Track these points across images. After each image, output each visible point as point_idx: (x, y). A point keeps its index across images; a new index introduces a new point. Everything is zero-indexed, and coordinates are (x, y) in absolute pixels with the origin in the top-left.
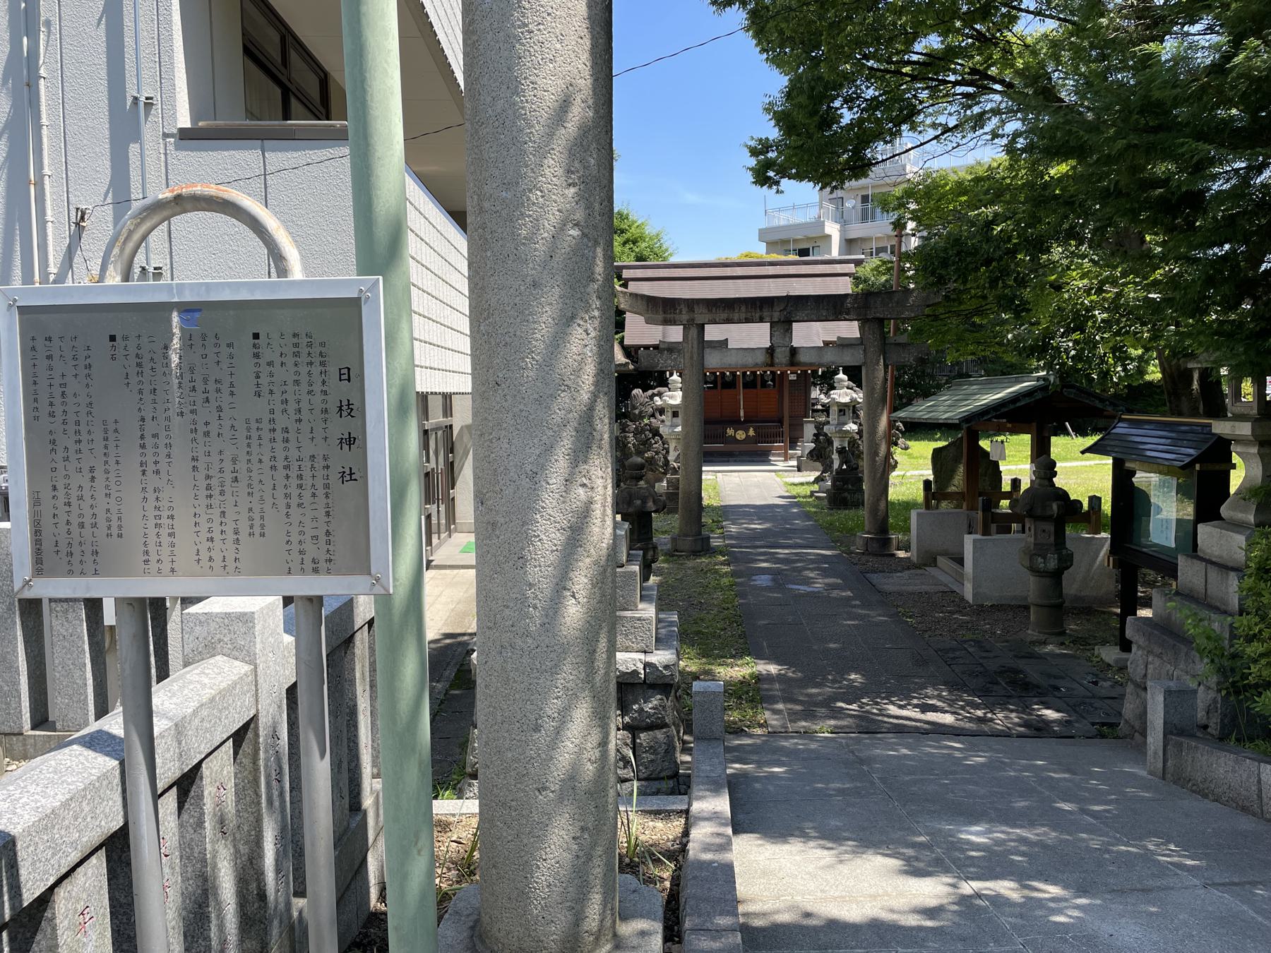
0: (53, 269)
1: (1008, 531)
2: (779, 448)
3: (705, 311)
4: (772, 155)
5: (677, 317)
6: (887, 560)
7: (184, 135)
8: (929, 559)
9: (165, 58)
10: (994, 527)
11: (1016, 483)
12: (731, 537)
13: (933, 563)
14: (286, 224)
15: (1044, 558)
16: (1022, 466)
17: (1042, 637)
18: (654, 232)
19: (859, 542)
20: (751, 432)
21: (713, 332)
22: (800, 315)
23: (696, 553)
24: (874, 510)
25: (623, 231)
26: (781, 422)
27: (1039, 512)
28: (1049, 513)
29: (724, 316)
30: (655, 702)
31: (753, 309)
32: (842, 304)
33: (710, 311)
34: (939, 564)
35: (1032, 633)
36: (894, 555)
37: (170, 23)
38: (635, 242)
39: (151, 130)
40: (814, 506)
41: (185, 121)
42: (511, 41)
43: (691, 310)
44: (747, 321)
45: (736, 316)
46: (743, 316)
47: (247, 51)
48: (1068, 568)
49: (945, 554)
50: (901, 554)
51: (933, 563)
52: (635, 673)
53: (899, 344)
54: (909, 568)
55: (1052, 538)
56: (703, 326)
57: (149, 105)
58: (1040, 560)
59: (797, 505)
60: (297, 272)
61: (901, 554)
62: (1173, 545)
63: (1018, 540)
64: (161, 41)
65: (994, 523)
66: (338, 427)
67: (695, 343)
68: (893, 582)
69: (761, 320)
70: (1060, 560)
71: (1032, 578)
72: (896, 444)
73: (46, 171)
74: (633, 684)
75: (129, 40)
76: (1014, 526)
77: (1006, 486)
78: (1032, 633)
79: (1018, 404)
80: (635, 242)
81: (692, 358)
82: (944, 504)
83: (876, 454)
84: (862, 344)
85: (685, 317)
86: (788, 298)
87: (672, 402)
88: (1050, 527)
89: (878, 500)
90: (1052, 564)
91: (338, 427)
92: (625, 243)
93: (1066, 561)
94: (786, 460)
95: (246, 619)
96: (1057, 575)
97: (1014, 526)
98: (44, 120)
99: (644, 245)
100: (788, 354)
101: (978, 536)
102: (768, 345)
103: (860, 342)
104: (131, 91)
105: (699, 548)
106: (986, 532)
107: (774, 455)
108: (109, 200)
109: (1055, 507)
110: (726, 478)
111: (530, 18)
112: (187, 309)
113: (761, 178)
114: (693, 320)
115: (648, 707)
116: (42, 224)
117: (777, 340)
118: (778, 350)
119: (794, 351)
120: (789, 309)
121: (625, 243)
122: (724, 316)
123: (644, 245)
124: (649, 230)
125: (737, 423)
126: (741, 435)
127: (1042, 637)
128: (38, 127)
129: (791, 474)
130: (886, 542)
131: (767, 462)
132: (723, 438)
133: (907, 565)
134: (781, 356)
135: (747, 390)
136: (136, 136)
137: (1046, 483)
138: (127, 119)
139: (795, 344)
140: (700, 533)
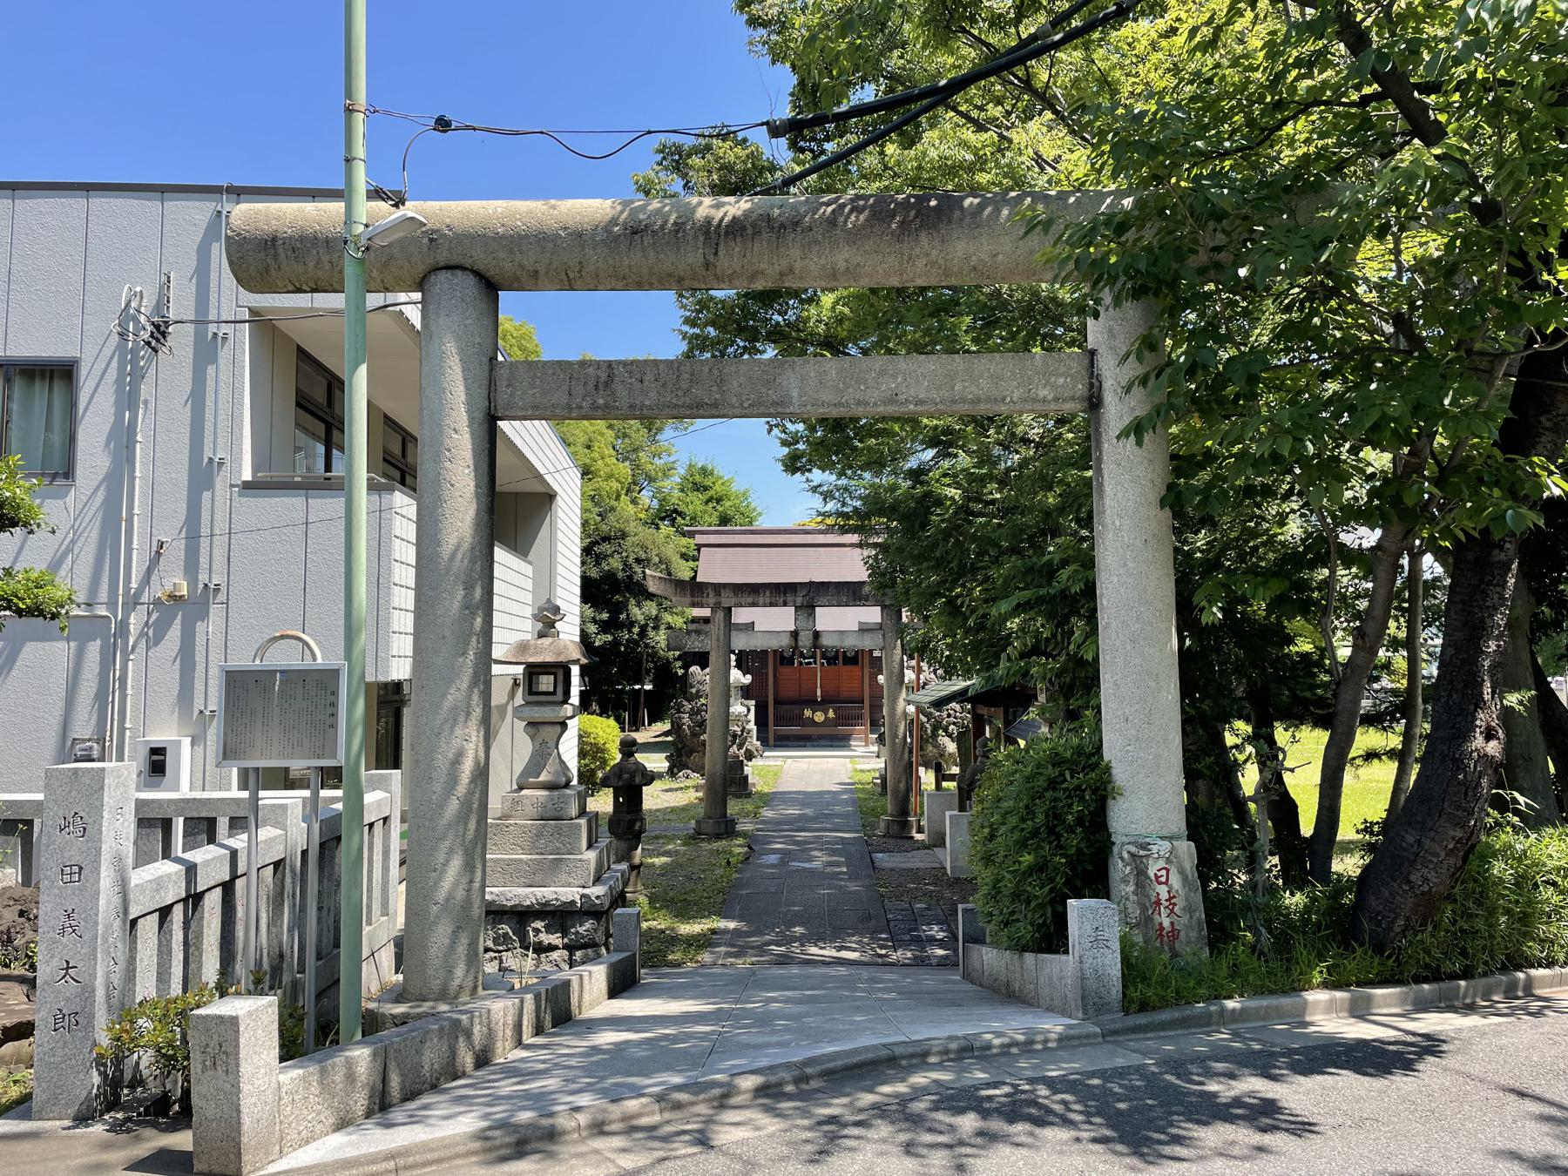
0: (134, 585)
2: (860, 732)
4: (801, 446)
7: (247, 486)
9: (236, 430)
12: (762, 822)
14: (318, 643)
18: (742, 489)
19: (882, 825)
20: (831, 714)
21: (741, 615)
22: (823, 600)
23: (718, 837)
25: (706, 489)
29: (750, 600)
30: (587, 925)
31: (778, 593)
33: (736, 595)
37: (242, 404)
38: (719, 500)
39: (221, 483)
41: (247, 475)
42: (437, 522)
43: (718, 594)
44: (772, 605)
45: (761, 600)
46: (768, 600)
47: (298, 404)
50: (919, 837)
52: (573, 902)
56: (729, 609)
57: (221, 464)
60: (319, 661)
61: (919, 837)
64: (235, 419)
66: (330, 710)
69: (785, 604)
73: (136, 511)
74: (572, 913)
75: (209, 416)
80: (719, 500)
85: (712, 600)
86: (811, 583)
91: (330, 710)
92: (707, 503)
95: (284, 807)
98: (138, 474)
99: (728, 504)
103: (880, 627)
104: (208, 453)
108: (183, 535)
111: (448, 512)
112: (282, 672)
115: (581, 930)
116: (129, 550)
119: (817, 635)
121: (707, 503)
122: (750, 600)
123: (728, 504)
124: (736, 487)
125: (812, 703)
126: (819, 717)
128: (132, 478)
130: (905, 825)
131: (847, 747)
133: (923, 846)
134: (805, 641)
136: (210, 486)
138: (202, 474)
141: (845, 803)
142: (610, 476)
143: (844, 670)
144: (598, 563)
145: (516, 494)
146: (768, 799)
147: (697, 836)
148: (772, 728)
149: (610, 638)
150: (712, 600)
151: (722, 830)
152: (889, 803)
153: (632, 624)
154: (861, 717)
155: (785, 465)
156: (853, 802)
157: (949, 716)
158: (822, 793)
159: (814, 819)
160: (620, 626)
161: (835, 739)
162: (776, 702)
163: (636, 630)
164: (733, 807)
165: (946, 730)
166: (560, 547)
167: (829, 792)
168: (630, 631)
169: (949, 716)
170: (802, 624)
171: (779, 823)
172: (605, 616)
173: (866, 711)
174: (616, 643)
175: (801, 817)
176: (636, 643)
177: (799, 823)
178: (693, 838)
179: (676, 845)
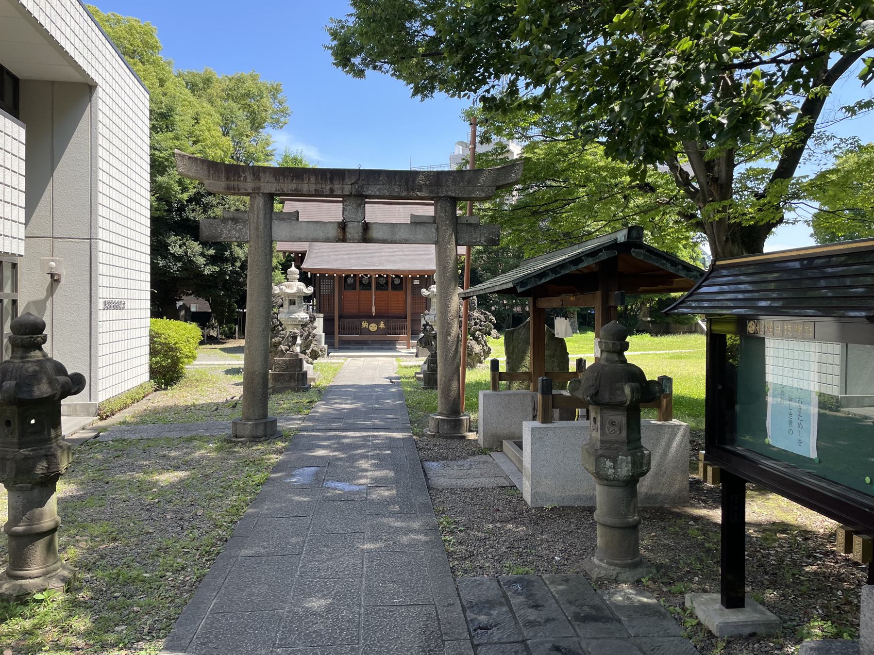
1: (571, 416)
3: (273, 180)
5: (241, 184)
6: (455, 443)
8: (495, 444)
10: (556, 412)
11: (580, 362)
13: (499, 448)
15: (614, 460)
16: (589, 355)
17: (613, 571)
19: (432, 424)
20: (382, 325)
23: (255, 439)
24: (446, 391)
26: (406, 317)
27: (606, 397)
28: (620, 399)
32: (414, 181)
33: (277, 180)
34: (504, 449)
35: (598, 565)
36: (464, 437)
40: (413, 386)
48: (644, 474)
49: (508, 438)
50: (472, 436)
51: (499, 448)
53: (471, 225)
54: (474, 454)
55: (624, 433)
58: (609, 463)
59: (399, 385)
61: (472, 436)
62: (814, 455)
63: (583, 431)
65: (553, 406)
67: (262, 212)
68: (445, 475)
70: (634, 463)
71: (598, 488)
72: (489, 334)
76: (579, 411)
77: (572, 367)
78: (598, 565)
79: (581, 266)
81: (257, 229)
82: (516, 385)
83: (449, 334)
84: (434, 222)
87: (289, 291)
88: (621, 418)
89: (450, 380)
90: (625, 470)
93: (640, 466)
94: (408, 348)
96: (631, 483)
97: (579, 411)
100: (360, 230)
101: (537, 424)
102: (340, 219)
103: (434, 220)
105: (260, 432)
106: (547, 419)
107: (400, 344)
109: (627, 390)
110: (354, 362)
113: (344, 55)
114: (259, 188)
117: (351, 215)
118: (350, 225)
120: (361, 183)
125: (369, 318)
126: (373, 327)
127: (613, 571)
129: (408, 359)
130: (456, 424)
131: (394, 349)
132: (359, 330)
135: (379, 292)
137: (615, 357)
139: (368, 220)
140: (265, 416)
141: (393, 396)
142: (216, 145)
143: (391, 293)
144: (205, 211)
145: (53, 83)
146: (324, 393)
147: (233, 440)
148: (337, 336)
149: (217, 269)
150: (250, 185)
151: (260, 432)
152: (436, 397)
153: (234, 260)
154: (404, 328)
155: (335, 54)
156: (401, 395)
157: (476, 324)
158: (372, 387)
159: (367, 414)
160: (226, 260)
161: (385, 344)
162: (340, 317)
163: (238, 264)
164: (280, 404)
165: (473, 335)
166: (101, 140)
167: (378, 386)
168: (233, 265)
169: (476, 324)
170: (351, 215)
171: (333, 419)
172: (212, 252)
173: (408, 323)
174: (222, 273)
175: (353, 413)
176: (237, 273)
177: (347, 420)
178: (228, 441)
179: (206, 451)
